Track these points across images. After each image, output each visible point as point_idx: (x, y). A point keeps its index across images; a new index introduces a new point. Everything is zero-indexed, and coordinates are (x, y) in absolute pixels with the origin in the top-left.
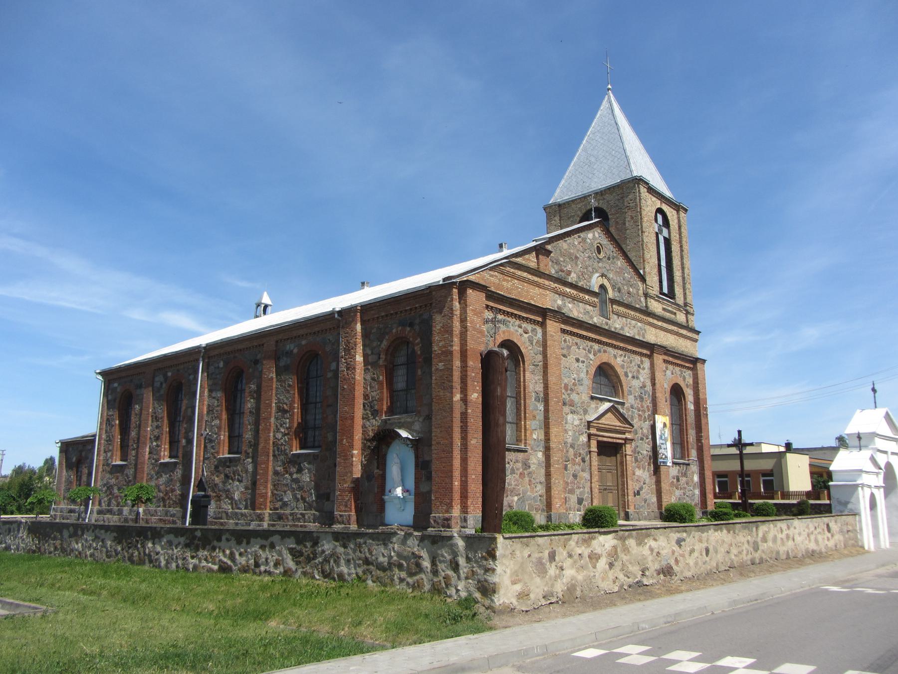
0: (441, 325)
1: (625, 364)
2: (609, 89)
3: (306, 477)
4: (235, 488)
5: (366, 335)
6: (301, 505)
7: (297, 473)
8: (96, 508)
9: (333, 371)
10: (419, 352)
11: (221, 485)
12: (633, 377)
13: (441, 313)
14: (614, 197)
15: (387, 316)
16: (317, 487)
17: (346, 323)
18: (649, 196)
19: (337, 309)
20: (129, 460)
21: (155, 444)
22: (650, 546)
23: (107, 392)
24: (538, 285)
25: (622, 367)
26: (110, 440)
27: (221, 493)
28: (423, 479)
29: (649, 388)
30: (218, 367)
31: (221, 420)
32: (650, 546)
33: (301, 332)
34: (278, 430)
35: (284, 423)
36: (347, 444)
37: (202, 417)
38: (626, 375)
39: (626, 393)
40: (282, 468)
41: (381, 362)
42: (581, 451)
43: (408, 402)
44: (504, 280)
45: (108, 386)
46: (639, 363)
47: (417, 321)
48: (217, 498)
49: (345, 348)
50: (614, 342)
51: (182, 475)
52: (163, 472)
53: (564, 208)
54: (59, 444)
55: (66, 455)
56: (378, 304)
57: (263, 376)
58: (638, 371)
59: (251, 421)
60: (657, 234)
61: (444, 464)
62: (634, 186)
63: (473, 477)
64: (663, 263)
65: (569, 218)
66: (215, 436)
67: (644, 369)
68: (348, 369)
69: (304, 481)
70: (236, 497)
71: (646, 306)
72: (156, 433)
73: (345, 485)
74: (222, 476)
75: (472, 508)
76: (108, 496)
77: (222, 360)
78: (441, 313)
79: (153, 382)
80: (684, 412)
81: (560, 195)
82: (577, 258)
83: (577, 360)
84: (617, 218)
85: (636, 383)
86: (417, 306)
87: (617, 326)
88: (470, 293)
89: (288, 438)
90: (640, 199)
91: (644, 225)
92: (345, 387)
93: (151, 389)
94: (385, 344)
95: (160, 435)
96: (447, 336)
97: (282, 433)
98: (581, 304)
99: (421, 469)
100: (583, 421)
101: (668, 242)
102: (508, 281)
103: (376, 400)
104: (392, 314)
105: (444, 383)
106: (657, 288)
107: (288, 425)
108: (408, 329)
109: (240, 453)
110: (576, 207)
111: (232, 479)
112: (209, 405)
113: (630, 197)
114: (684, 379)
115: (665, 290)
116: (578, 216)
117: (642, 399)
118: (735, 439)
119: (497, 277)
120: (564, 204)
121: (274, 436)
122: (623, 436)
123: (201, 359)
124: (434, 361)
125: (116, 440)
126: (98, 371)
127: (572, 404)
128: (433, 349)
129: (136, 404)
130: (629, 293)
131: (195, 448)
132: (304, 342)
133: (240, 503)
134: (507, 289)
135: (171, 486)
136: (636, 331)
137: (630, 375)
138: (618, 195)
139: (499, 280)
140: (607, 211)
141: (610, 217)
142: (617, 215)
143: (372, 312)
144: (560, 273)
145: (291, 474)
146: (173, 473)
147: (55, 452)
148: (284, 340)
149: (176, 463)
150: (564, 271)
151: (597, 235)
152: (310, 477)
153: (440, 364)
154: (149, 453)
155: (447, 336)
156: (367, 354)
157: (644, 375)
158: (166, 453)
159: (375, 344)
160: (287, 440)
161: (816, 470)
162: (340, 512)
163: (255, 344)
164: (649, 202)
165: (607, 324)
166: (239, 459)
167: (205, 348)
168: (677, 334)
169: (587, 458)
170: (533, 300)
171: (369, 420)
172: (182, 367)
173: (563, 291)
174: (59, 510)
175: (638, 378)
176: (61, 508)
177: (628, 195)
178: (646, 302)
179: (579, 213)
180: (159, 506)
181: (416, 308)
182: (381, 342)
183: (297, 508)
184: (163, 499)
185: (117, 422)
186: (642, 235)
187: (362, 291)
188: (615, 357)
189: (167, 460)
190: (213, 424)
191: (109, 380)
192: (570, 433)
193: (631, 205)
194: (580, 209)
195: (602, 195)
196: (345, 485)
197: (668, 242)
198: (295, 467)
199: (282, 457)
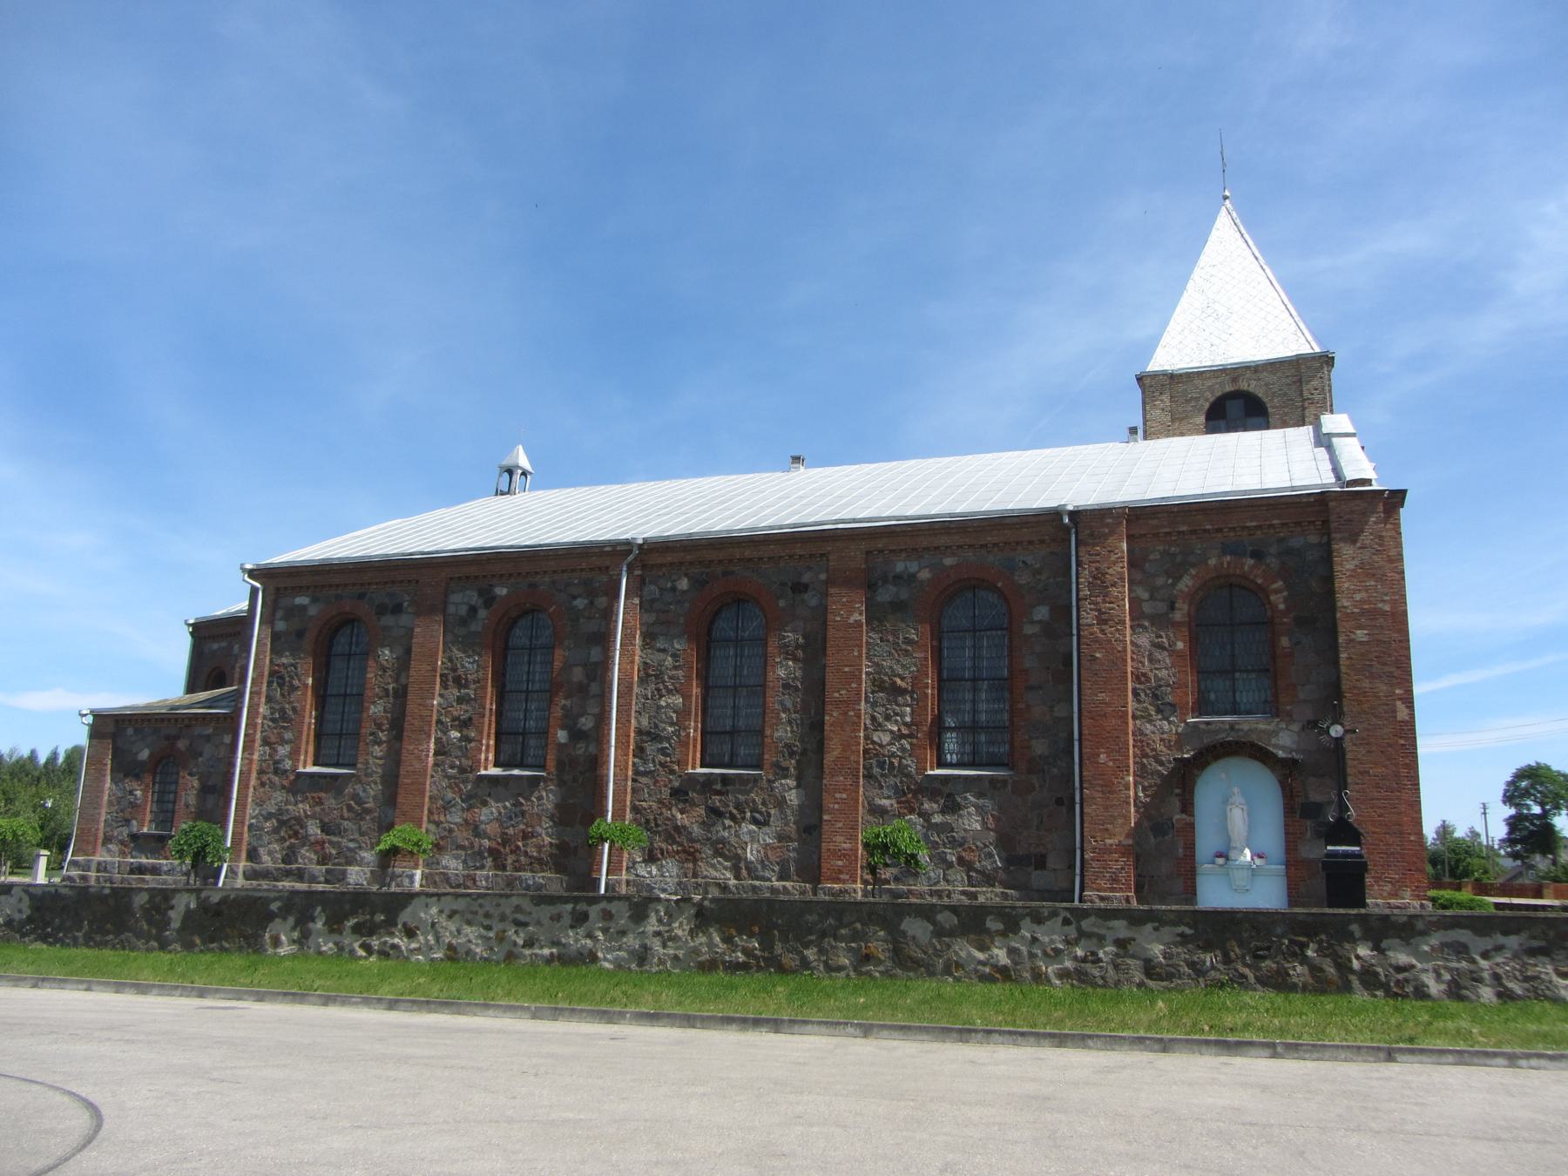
0: (1356, 562)
2: (1226, 198)
3: (971, 822)
4: (747, 838)
5: (1135, 562)
6: (958, 875)
7: (943, 812)
8: (243, 865)
9: (1040, 622)
10: (1282, 607)
11: (696, 830)
13: (1354, 542)
14: (1279, 378)
15: (1193, 532)
16: (1005, 842)
17: (1092, 535)
19: (1070, 508)
20: (359, 766)
21: (455, 734)
22: (405, 925)
23: (273, 614)
26: (284, 717)
27: (698, 846)
28: (1309, 834)
30: (674, 589)
31: (687, 697)
32: (405, 925)
33: (943, 540)
34: (878, 726)
35: (897, 714)
36: (1111, 764)
37: (630, 688)
40: (894, 802)
41: (1178, 616)
43: (1237, 694)
45: (275, 601)
47: (1273, 550)
49: (1089, 583)
51: (557, 806)
52: (489, 795)
53: (1178, 383)
54: (90, 719)
55: (114, 743)
56: (1176, 510)
57: (830, 617)
59: (789, 704)
61: (1379, 811)
62: (1322, 368)
65: (1188, 401)
66: (670, 729)
68: (1102, 621)
69: (965, 830)
70: (751, 854)
72: (460, 711)
73: (1109, 841)
74: (701, 811)
76: (283, 840)
77: (686, 575)
78: (1354, 542)
79: (445, 603)
81: (1166, 359)
84: (1286, 414)
86: (1276, 522)
89: (911, 744)
92: (1098, 655)
93: (439, 618)
94: (1186, 583)
95: (475, 718)
96: (1373, 583)
97: (892, 732)
99: (1301, 817)
103: (1169, 685)
104: (1206, 531)
105: (1371, 666)
107: (908, 719)
108: (1251, 562)
109: (758, 766)
110: (1203, 385)
111: (733, 818)
112: (645, 663)
113: (1315, 383)
116: (1207, 400)
118: (33, 756)
120: (1181, 375)
121: (867, 738)
123: (625, 568)
124: (1342, 627)
125: (307, 720)
126: (248, 566)
128: (1339, 604)
129: (383, 646)
131: (613, 749)
132: (948, 561)
133: (764, 867)
135: (522, 827)
138: (1287, 377)
140: (1265, 400)
141: (1270, 410)
142: (1286, 410)
143: (1155, 522)
145: (925, 815)
146: (528, 799)
147: (80, 736)
148: (891, 551)
149: (534, 782)
152: (984, 823)
153: (1358, 632)
154: (435, 754)
155: (1373, 583)
156: (1138, 597)
158: (491, 757)
159: (1160, 581)
160: (908, 747)
162: (1098, 891)
163: (799, 552)
166: (756, 779)
167: (640, 546)
171: (1150, 721)
172: (547, 579)
174: (94, 867)
176: (99, 864)
177: (1310, 381)
179: (1208, 395)
180: (482, 867)
181: (1271, 526)
182: (1178, 579)
183: (947, 881)
184: (494, 853)
185: (310, 681)
187: (785, 476)
189: (494, 771)
190: (663, 703)
191: (278, 589)
193: (1316, 397)
194: (1211, 389)
195: (1256, 371)
196: (1109, 841)
198: (936, 802)
199: (891, 781)
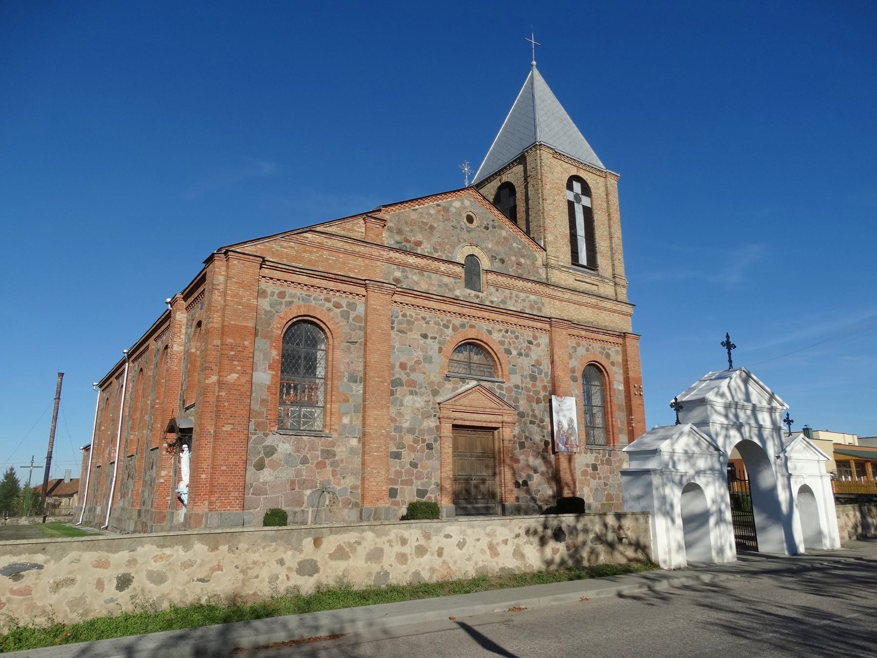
1: (506, 340)
12: (520, 354)
18: (555, 162)
24: (362, 256)
25: (502, 343)
29: (546, 365)
38: (508, 352)
39: (506, 372)
42: (426, 437)
44: (305, 251)
46: (531, 339)
48: (744, 375)
50: (192, 285)
58: (530, 348)
60: (571, 205)
63: (224, 468)
64: (581, 231)
67: (538, 345)
71: (547, 279)
75: (219, 504)
80: (608, 392)
82: (432, 228)
83: (425, 336)
85: (525, 363)
87: (495, 299)
88: (235, 265)
90: (541, 166)
91: (546, 192)
98: (433, 276)
100: (431, 403)
101: (588, 213)
102: (311, 252)
106: (565, 257)
114: (608, 356)
115: (583, 259)
117: (533, 378)
119: (293, 248)
122: (500, 418)
127: (412, 383)
130: (519, 264)
134: (309, 261)
136: (527, 304)
137: (514, 353)
139: (297, 252)
144: (404, 243)
150: (410, 242)
151: (467, 203)
157: (540, 352)
161: (842, 457)
164: (558, 169)
165: (478, 297)
168: (596, 307)
169: (436, 445)
170: (354, 272)
173: (402, 262)
175: (527, 355)
178: (547, 273)
186: (543, 203)
188: (490, 332)
192: (407, 417)
197: (588, 213)
